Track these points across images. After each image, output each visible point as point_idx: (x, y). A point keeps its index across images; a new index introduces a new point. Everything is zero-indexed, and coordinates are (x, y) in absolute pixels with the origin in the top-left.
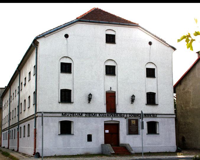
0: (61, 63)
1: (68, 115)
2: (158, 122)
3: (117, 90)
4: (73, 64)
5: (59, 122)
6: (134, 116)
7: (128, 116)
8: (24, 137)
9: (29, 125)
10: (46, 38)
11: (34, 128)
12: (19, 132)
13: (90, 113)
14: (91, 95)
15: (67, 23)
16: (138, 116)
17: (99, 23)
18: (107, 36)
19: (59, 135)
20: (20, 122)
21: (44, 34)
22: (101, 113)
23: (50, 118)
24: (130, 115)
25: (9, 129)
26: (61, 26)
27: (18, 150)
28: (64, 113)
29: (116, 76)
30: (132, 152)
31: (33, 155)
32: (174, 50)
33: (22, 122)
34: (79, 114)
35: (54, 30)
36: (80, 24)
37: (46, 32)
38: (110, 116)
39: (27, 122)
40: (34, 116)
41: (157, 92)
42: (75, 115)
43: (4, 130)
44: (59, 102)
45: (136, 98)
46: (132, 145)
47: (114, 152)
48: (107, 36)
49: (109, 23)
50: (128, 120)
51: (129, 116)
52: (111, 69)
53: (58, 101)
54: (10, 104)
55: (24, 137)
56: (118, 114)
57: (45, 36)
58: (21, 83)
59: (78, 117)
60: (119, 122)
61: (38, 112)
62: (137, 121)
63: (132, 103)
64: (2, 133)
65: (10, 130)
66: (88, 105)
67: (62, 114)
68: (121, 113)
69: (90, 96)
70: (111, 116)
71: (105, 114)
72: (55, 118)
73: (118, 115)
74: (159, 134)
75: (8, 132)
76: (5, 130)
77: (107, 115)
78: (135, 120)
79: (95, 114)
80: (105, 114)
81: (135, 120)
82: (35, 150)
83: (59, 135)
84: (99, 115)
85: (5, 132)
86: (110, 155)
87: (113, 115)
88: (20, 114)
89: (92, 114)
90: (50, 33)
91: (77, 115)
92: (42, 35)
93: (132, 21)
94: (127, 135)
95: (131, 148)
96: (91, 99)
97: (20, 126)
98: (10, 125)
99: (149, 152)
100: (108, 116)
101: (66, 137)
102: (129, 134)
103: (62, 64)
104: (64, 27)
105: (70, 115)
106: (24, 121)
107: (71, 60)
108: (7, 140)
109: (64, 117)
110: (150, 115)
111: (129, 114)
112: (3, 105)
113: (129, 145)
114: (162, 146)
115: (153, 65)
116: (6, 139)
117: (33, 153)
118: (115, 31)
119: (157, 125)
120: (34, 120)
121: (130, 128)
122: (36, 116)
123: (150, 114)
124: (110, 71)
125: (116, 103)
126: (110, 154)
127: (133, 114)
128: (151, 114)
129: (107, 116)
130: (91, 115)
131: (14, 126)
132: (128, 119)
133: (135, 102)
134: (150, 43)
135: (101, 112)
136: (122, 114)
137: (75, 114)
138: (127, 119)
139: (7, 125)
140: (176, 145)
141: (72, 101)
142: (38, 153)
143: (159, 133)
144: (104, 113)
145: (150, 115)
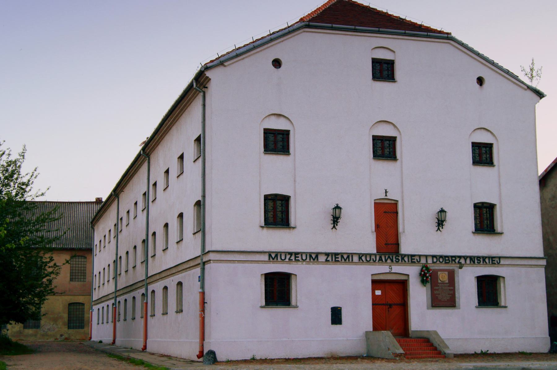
1: (283, 258)
2: (504, 278)
4: (294, 134)
6: (446, 263)
8: (163, 314)
9: (180, 284)
11: (201, 290)
12: (147, 303)
13: (336, 254)
15: (277, 32)
16: (454, 260)
17: (355, 30)
18: (376, 62)
19: (262, 307)
20: (149, 279)
21: (222, 59)
22: (363, 255)
23: (240, 265)
24: (435, 260)
25: (116, 297)
26: (262, 38)
27: (145, 347)
28: (273, 252)
29: (398, 162)
30: (447, 351)
31: (196, 359)
32: (538, 98)
33: (157, 277)
34: (311, 256)
35: (247, 48)
36: (308, 34)
37: (228, 53)
39: (172, 278)
40: (198, 261)
41: (500, 202)
42: (300, 259)
43: (100, 301)
44: (262, 227)
45: (449, 216)
46: (443, 335)
47: (401, 351)
48: (376, 62)
49: (379, 31)
51: (433, 262)
52: (386, 143)
54: (116, 237)
55: (165, 313)
56: (405, 255)
57: (226, 64)
58: (152, 183)
59: (308, 263)
60: (408, 275)
61: (209, 252)
62: (452, 275)
63: (439, 229)
64: (94, 307)
65: (118, 299)
66: (331, 233)
67: (270, 256)
68: (413, 253)
70: (389, 261)
71: (373, 257)
72: (250, 265)
73: (406, 259)
74: (506, 307)
75: (113, 304)
76: (103, 299)
79: (348, 257)
80: (373, 257)
81: (447, 273)
82: (202, 346)
83: (262, 307)
84: (360, 258)
85: (104, 304)
86: (318, 363)
87: (394, 260)
88: (150, 259)
89: (342, 257)
90: (237, 56)
91: (304, 258)
92: (218, 61)
93: (433, 27)
94: (428, 308)
95: (442, 341)
97: (151, 288)
98: (118, 289)
99: (288, 358)
100: (382, 260)
101: (279, 312)
103: (268, 132)
104: (272, 40)
105: (289, 259)
106: (163, 275)
107: (288, 121)
108: (111, 325)
109: (273, 262)
110: (484, 260)
111: (433, 256)
112: (96, 242)
113: (435, 333)
114: (514, 337)
115: (391, 127)
116: (101, 321)
117: (198, 353)
118: (394, 52)
119: (502, 285)
120: (198, 270)
121: (436, 292)
122: (204, 260)
123: (484, 258)
124: (383, 148)
126: (392, 356)
127: (441, 257)
128: (486, 257)
130: (340, 259)
131: (131, 288)
134: (480, 81)
135: (363, 252)
136: (414, 256)
137: (299, 256)
139: (109, 288)
140: (548, 336)
141: (292, 223)
142: (212, 353)
144: (370, 255)
145: (484, 260)
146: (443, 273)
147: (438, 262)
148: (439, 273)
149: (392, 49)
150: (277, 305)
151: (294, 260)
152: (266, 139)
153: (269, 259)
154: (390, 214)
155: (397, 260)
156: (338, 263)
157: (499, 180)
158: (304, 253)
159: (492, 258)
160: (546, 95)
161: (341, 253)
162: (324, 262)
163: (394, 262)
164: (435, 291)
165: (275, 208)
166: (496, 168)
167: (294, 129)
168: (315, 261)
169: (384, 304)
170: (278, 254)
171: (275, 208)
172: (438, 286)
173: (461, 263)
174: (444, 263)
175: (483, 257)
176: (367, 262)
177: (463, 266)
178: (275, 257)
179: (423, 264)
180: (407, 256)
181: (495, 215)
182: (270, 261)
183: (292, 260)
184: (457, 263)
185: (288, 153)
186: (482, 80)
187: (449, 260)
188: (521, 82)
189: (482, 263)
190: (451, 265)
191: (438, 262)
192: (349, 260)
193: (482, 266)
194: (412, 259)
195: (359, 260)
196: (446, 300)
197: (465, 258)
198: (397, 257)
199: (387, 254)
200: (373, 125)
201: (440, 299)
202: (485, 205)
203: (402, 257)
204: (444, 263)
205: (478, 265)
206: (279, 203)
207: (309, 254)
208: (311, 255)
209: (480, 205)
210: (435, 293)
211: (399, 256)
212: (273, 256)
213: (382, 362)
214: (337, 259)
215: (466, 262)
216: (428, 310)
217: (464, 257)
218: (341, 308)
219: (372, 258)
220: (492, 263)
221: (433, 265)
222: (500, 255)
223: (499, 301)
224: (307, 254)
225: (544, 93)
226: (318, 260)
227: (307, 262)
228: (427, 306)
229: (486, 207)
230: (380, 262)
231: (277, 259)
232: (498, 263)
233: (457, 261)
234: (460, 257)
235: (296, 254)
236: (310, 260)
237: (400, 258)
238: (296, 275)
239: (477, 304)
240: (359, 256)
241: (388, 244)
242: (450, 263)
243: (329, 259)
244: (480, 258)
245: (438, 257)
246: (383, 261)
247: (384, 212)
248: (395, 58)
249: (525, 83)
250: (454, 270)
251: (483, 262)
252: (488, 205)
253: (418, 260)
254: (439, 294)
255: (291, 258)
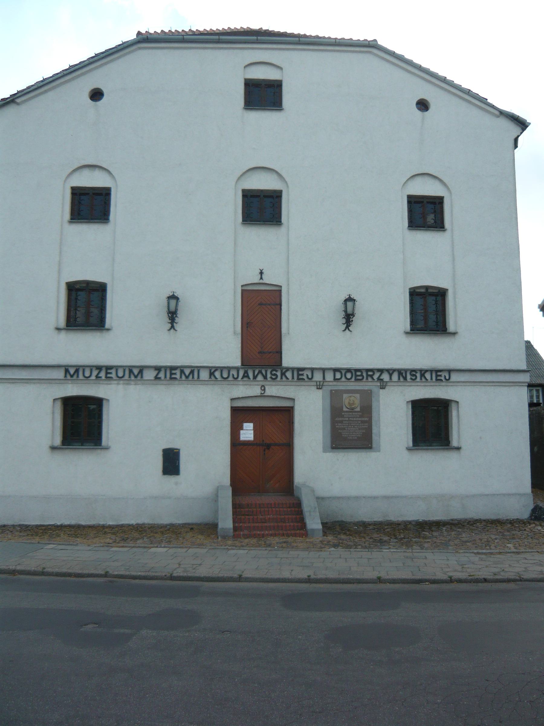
0: (73, 189)
1: (87, 374)
2: (457, 402)
3: (288, 281)
5: (55, 400)
6: (356, 380)
7: (329, 376)
10: (23, 107)
14: (177, 299)
16: (371, 376)
22: (216, 368)
24: (338, 376)
29: (283, 229)
34: (131, 372)
38: (255, 377)
41: (454, 287)
42: (113, 375)
44: (407, 333)
50: (328, 394)
51: (335, 379)
53: (53, 325)
56: (288, 369)
57: (18, 100)
67: (67, 371)
69: (350, 304)
70: (260, 378)
71: (234, 372)
77: (241, 373)
78: (358, 396)
79: (192, 372)
81: (358, 396)
83: (53, 448)
84: (212, 374)
87: (269, 375)
89: (182, 372)
91: (120, 374)
94: (325, 451)
96: (353, 315)
100: (248, 377)
102: (333, 448)
105: (97, 377)
110: (423, 375)
111: (335, 370)
115: (437, 183)
118: (281, 68)
122: (324, 384)
123: (423, 372)
125: (284, 330)
127: (349, 370)
128: (426, 371)
129: (244, 377)
130: (178, 376)
132: (330, 388)
133: (181, 319)
134: (423, 105)
135: (217, 365)
136: (303, 369)
138: (327, 389)
141: (451, 327)
143: (459, 442)
144: (229, 369)
145: (423, 375)
146: (350, 397)
147: (343, 379)
148: (345, 396)
149: (278, 64)
150: (82, 445)
151: (104, 378)
152: (105, 203)
153: (65, 376)
154: (269, 306)
155: (274, 377)
156: (177, 382)
157: (453, 251)
158: (224, 368)
159: (437, 371)
160: (530, 124)
161: (182, 367)
162: (95, 380)
163: (269, 379)
164: (337, 424)
165: (425, 308)
166: (447, 234)
167: (117, 185)
168: (138, 379)
169: (257, 444)
170: (79, 369)
171: (425, 308)
172: (343, 416)
173: (382, 380)
174: (353, 379)
175: (421, 371)
176: (223, 379)
177: (386, 386)
178: (74, 374)
179: (317, 382)
180: (396, 371)
181: (447, 305)
182: (182, 380)
183: (100, 377)
184: (376, 380)
185: (443, 229)
186: (428, 106)
187: (362, 375)
188: (491, 106)
189: (418, 379)
190: (367, 384)
191: (343, 379)
192: (193, 377)
193: (419, 384)
194: (299, 375)
195: (210, 377)
196: (356, 438)
197: (390, 372)
198: (274, 372)
199: (263, 368)
200: (241, 176)
201: (346, 436)
202: (430, 291)
203: (282, 371)
204: (353, 379)
205: (413, 384)
206: (431, 300)
207: (129, 369)
208: (68, 368)
209: (423, 290)
210: (337, 427)
211: (417, 371)
212: (72, 371)
213: (344, 535)
214: (173, 376)
215: (391, 378)
216: (324, 453)
217: (388, 370)
218: (179, 450)
219: (231, 373)
220: (437, 380)
221: (335, 383)
222: (452, 366)
223: (450, 440)
224: (124, 368)
225: (526, 120)
226: (142, 377)
227: (126, 380)
228: (323, 448)
229: (432, 294)
230: (245, 379)
231: (78, 376)
232: (447, 380)
233: (376, 377)
234: (381, 371)
235: (108, 368)
236: (130, 377)
237: (279, 374)
238: (458, 402)
239: (411, 444)
240: (210, 371)
241: (264, 353)
242: (365, 380)
243: (162, 375)
244: (416, 373)
245: (343, 372)
246: (249, 378)
247: (259, 305)
248: (283, 77)
249: (497, 108)
250: (371, 390)
251: (421, 379)
252: (437, 291)
253: (310, 377)
254: (344, 429)
255: (159, 376)
